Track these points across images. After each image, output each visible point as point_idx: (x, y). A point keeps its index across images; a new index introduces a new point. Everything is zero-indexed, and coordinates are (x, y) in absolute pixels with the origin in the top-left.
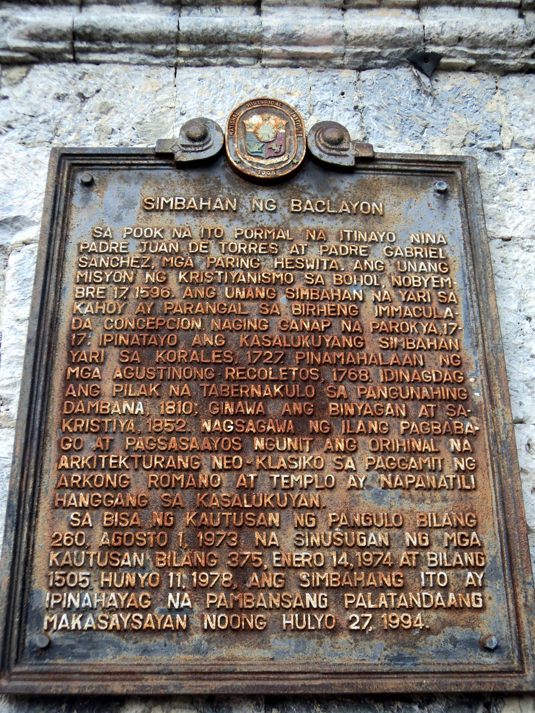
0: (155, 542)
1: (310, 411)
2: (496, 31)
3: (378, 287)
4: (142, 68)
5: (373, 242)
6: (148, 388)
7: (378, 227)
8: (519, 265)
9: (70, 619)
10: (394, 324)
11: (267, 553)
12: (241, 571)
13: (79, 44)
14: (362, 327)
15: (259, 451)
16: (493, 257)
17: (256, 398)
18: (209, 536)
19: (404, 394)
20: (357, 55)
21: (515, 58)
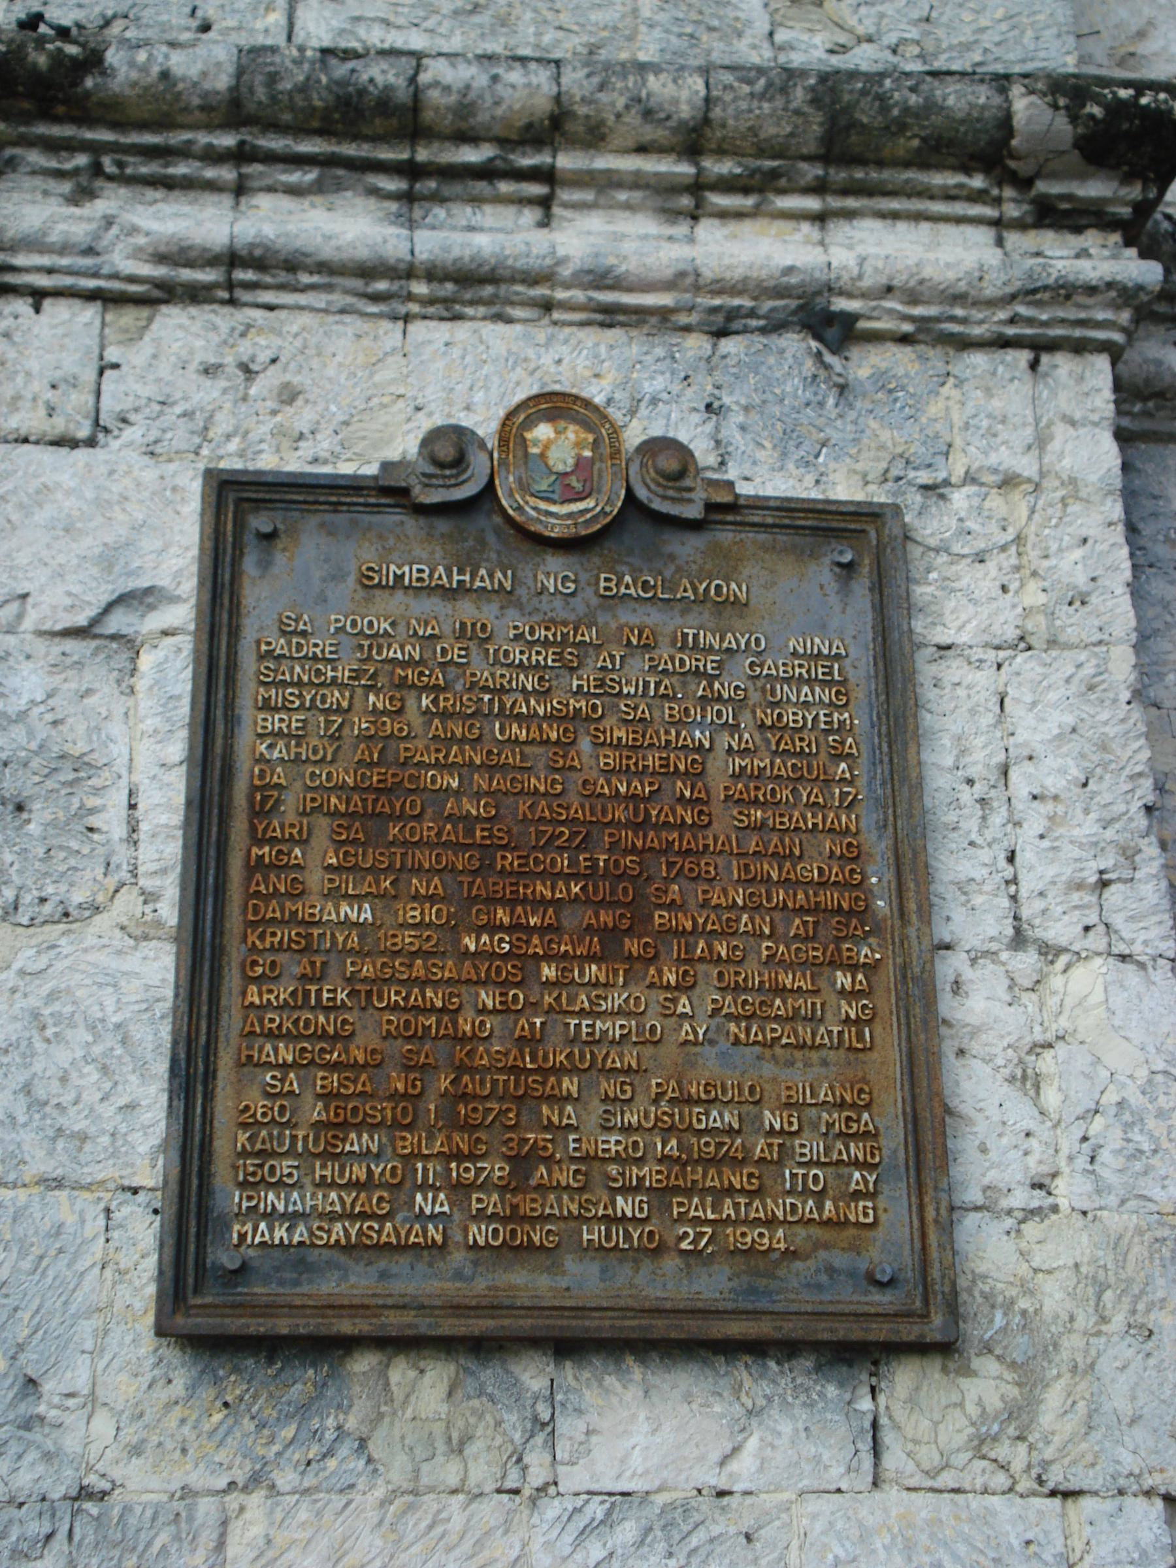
0: (394, 1119)
1: (625, 924)
2: (951, 275)
3: (734, 728)
4: (348, 319)
5: (728, 650)
6: (378, 882)
7: (738, 624)
8: (961, 692)
9: (271, 1229)
10: (757, 788)
11: (560, 1136)
12: (522, 1163)
13: (241, 275)
14: (707, 793)
15: (548, 984)
16: (920, 678)
17: (543, 902)
18: (475, 1110)
19: (769, 900)
20: (715, 310)
21: (981, 322)
